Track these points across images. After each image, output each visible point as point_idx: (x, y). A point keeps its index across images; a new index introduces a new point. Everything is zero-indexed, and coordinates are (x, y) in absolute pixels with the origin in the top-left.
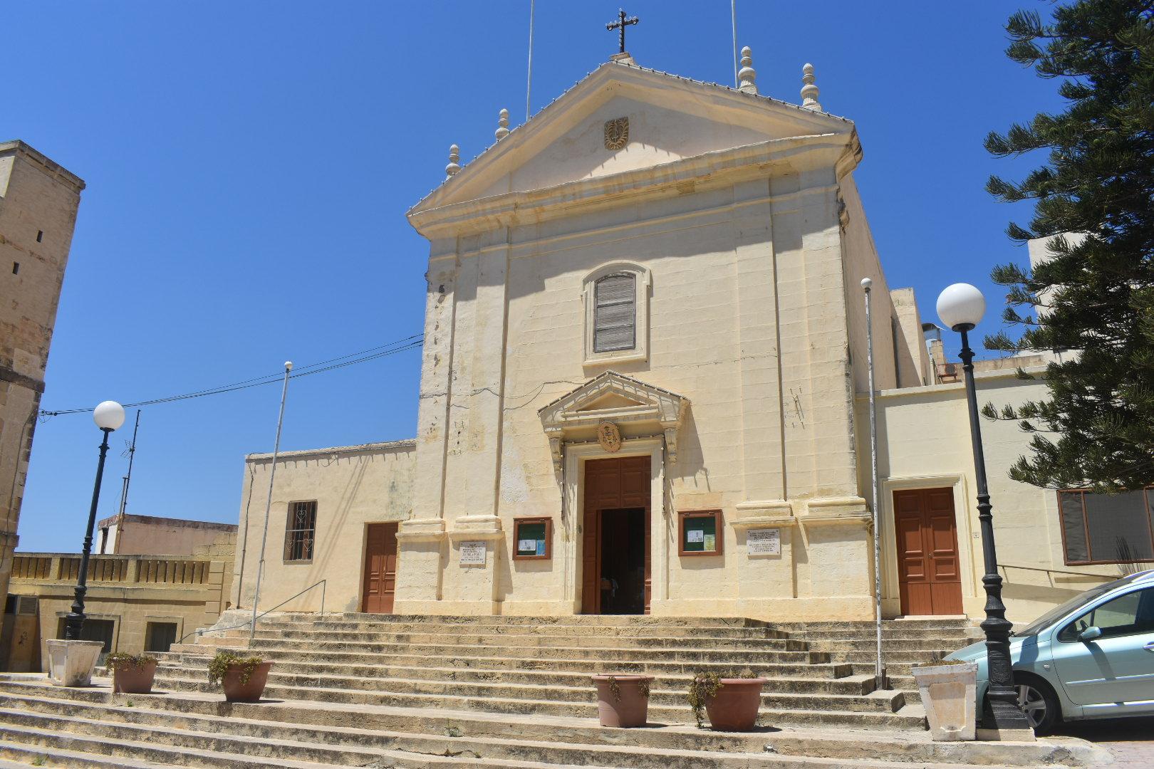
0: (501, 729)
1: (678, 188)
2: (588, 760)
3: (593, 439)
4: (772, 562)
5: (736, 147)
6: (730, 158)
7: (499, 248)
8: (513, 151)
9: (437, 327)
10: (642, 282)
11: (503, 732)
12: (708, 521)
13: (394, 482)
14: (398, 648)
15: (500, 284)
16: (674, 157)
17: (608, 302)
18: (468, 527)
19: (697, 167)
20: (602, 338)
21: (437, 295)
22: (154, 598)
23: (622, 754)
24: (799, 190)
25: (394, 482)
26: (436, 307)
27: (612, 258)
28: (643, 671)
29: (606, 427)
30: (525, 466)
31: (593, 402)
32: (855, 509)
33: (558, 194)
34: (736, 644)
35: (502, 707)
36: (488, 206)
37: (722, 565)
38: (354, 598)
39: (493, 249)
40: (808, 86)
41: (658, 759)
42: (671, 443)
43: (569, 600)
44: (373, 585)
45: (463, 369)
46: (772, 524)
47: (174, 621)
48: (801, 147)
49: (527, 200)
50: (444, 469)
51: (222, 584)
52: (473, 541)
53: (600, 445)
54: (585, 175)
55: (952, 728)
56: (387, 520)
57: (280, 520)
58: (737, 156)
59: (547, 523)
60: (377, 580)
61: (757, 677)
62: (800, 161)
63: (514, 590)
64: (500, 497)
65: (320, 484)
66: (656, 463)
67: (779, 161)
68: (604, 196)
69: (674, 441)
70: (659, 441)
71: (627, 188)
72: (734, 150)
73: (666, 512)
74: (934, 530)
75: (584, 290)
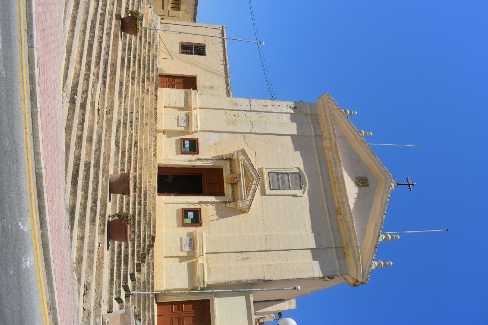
0: (109, 133)
1: (339, 208)
2: (96, 169)
3: (232, 172)
4: (179, 247)
6: (352, 230)
8: (354, 138)
9: (279, 106)
10: (298, 192)
11: (108, 134)
12: (197, 220)
13: (213, 88)
15: (297, 133)
16: (352, 206)
17: (290, 178)
18: (194, 119)
20: (275, 176)
21: (293, 106)
24: (338, 260)
26: (288, 106)
29: (237, 177)
30: (220, 143)
31: (248, 172)
32: (202, 282)
33: (336, 157)
34: (144, 232)
35: (118, 133)
36: (331, 127)
37: (178, 226)
38: (165, 71)
39: (312, 129)
42: (230, 205)
43: (164, 162)
45: (261, 117)
46: (196, 248)
48: (356, 260)
49: (333, 144)
51: (171, 16)
52: (189, 121)
54: (345, 169)
56: (198, 85)
57: (198, 40)
59: (196, 152)
60: (172, 81)
62: (350, 260)
63: (168, 138)
64: (208, 133)
65: (213, 57)
66: (221, 199)
68: (335, 176)
69: (231, 206)
73: (201, 203)
74: (193, 316)
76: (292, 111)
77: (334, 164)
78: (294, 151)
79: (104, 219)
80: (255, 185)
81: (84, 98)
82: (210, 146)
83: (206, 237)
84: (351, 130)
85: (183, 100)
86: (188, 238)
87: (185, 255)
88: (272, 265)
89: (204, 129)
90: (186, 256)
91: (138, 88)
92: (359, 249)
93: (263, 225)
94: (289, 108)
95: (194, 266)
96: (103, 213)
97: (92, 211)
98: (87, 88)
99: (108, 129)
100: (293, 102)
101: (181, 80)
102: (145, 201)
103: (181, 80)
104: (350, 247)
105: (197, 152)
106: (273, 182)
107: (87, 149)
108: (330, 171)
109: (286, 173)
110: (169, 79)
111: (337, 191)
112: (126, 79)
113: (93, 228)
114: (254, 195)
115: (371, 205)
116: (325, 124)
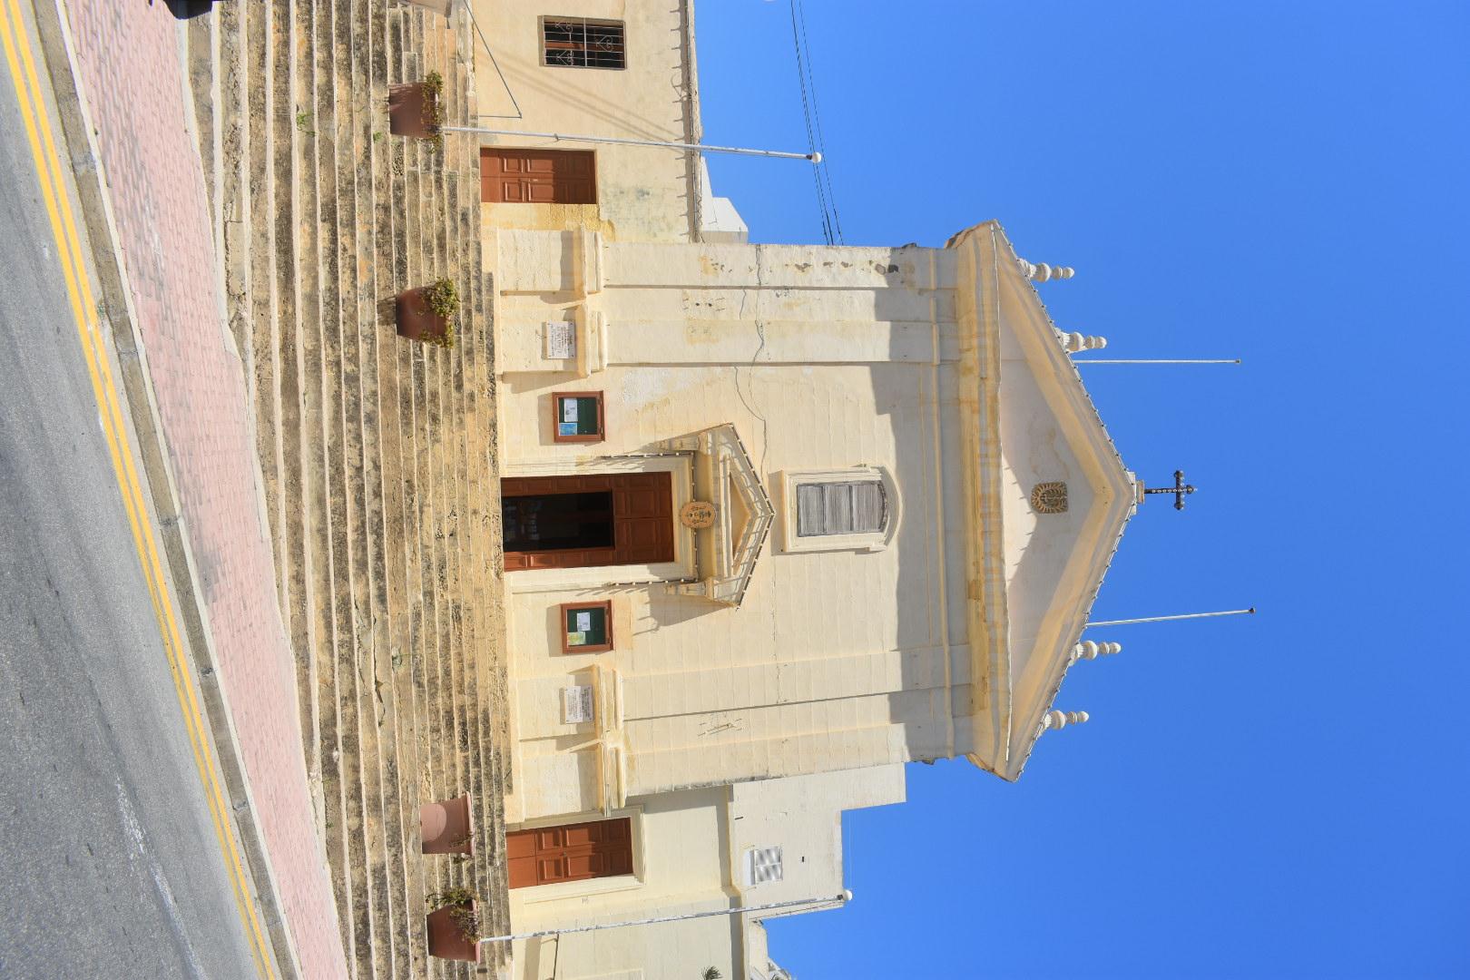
1: (976, 581)
2: (393, 850)
3: (696, 496)
6: (999, 648)
7: (935, 350)
8: (1050, 368)
9: (845, 265)
10: (873, 539)
11: (404, 722)
12: (600, 636)
13: (648, 194)
14: (461, 415)
15: (890, 356)
16: (1010, 571)
17: (854, 499)
18: (592, 332)
19: (995, 607)
20: (813, 494)
21: (886, 263)
24: (954, 717)
25: (648, 194)
26: (871, 262)
27: (906, 501)
28: (461, 751)
29: (709, 514)
30: (667, 402)
31: (740, 494)
32: (614, 798)
33: (990, 435)
35: (418, 646)
36: (989, 342)
37: (551, 654)
39: (935, 342)
40: (1063, 718)
42: (688, 590)
44: (514, 162)
45: (789, 306)
46: (598, 715)
48: (999, 725)
49: (989, 394)
50: (664, 287)
53: (689, 500)
54: (1009, 462)
58: (1000, 656)
60: (520, 169)
61: (437, 685)
62: (984, 720)
64: (630, 368)
65: (649, 73)
66: (666, 569)
67: (988, 699)
68: (979, 492)
69: (691, 593)
70: (691, 572)
71: (984, 523)
73: (610, 586)
76: (881, 282)
79: (422, 945)
81: (348, 719)
83: (624, 681)
84: (1045, 344)
86: (579, 688)
92: (1009, 699)
93: (772, 637)
94: (874, 272)
97: (398, 953)
98: (351, 687)
100: (889, 250)
104: (988, 689)
106: (807, 514)
107: (372, 830)
114: (754, 567)
115: (1062, 563)
116: (975, 329)
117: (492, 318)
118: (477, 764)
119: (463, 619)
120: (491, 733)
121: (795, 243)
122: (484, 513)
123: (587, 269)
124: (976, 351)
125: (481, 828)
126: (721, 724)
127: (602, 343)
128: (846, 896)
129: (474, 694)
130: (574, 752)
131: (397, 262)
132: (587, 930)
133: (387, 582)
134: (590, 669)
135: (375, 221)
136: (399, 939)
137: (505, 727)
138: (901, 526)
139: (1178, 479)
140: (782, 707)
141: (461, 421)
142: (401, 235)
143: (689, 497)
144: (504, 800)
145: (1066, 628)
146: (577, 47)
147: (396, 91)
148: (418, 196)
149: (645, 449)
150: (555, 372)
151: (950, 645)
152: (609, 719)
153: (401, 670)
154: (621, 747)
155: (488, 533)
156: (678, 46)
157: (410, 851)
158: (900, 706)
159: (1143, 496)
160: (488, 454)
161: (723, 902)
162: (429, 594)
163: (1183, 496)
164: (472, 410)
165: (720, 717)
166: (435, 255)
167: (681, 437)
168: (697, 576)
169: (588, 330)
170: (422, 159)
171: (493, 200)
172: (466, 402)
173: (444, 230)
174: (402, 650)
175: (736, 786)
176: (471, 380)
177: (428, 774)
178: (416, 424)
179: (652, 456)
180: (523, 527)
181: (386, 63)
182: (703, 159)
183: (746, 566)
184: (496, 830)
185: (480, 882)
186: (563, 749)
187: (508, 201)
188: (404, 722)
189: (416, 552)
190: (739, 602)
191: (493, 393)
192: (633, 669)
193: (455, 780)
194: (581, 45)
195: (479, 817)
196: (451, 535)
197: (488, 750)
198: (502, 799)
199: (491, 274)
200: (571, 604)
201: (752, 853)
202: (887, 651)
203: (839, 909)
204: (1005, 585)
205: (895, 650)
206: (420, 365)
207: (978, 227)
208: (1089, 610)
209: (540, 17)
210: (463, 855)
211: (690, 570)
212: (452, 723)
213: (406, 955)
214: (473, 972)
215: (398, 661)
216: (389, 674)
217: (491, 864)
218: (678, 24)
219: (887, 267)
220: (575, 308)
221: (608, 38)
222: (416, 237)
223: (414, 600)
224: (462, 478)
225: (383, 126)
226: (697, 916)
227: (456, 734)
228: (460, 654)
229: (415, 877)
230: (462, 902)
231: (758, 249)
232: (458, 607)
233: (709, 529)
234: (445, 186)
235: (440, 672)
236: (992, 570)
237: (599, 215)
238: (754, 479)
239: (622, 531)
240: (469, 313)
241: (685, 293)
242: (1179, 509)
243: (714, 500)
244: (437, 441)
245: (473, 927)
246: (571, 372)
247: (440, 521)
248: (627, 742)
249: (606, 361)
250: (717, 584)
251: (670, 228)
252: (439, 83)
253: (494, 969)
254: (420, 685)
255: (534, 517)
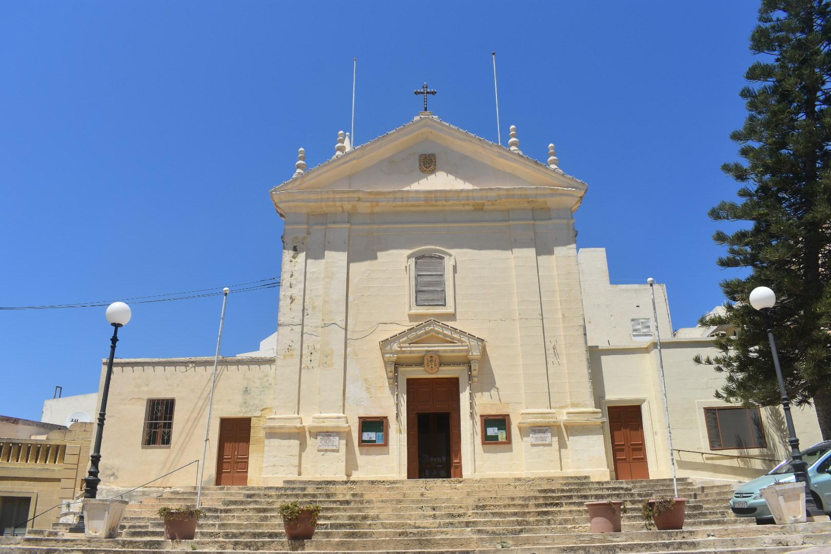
0: (539, 540)
1: (473, 205)
3: (421, 364)
4: (546, 448)
5: (517, 187)
6: (512, 193)
8: (355, 161)
9: (292, 276)
10: (448, 263)
11: (541, 541)
12: (502, 422)
13: (247, 388)
14: (364, 501)
15: (344, 251)
16: (468, 186)
17: (425, 273)
18: (324, 422)
20: (422, 296)
21: (292, 253)
22: (8, 476)
23: (639, 545)
24: (551, 219)
25: (247, 388)
26: (291, 261)
28: (562, 507)
29: (431, 357)
30: (366, 380)
33: (391, 196)
35: (498, 532)
36: (338, 196)
37: (511, 451)
38: (211, 475)
39: (337, 226)
40: (552, 158)
41: (661, 545)
42: (475, 370)
43: (403, 475)
44: (225, 465)
45: (314, 308)
46: (546, 424)
47: (27, 495)
48: (555, 194)
49: (368, 197)
51: (78, 464)
52: (328, 432)
54: (407, 186)
55: (795, 517)
56: (241, 415)
57: (139, 413)
58: (516, 192)
59: (384, 420)
60: (229, 462)
61: (522, 520)
62: (553, 202)
63: (359, 468)
64: (346, 401)
65: (178, 385)
67: (541, 200)
68: (423, 203)
69: (477, 368)
72: (515, 188)
73: (472, 415)
74: (630, 430)
75: (408, 263)
76: (302, 256)
77: (402, 201)
78: (377, 260)
79: (675, 534)
80: (444, 329)
82: (371, 397)
83: (527, 408)
85: (285, 442)
87: (557, 440)
88: (563, 315)
89: (340, 406)
90: (559, 438)
91: (372, 509)
92: (540, 188)
94: (296, 260)
95: (572, 427)
96: (667, 535)
97: (680, 548)
99: (533, 542)
100: (284, 251)
101: (227, 446)
102: (556, 491)
103: (227, 446)
104: (535, 199)
105: (506, 417)
108: (412, 209)
109: (416, 279)
110: (224, 468)
111: (448, 203)
112: (380, 528)
113: (703, 544)
116: (331, 203)
117: (310, 481)
118: (570, 497)
119: (484, 504)
120: (553, 488)
121: (278, 304)
122: (423, 490)
123: (287, 424)
124: (344, 203)
125: (609, 496)
126: (553, 352)
127: (331, 417)
128: (650, 281)
129: (529, 498)
130: (568, 438)
131: (270, 538)
132: (670, 433)
133: (456, 550)
134: (520, 428)
135: (243, 551)
136: (671, 547)
137: (550, 480)
138: (441, 247)
139: (419, 93)
140: (544, 316)
141: (368, 502)
142: (255, 535)
143: (422, 368)
144: (593, 481)
145: (501, 155)
146: (161, 426)
147: (168, 535)
148: (233, 524)
149: (393, 393)
150: (347, 445)
151: (509, 220)
152: (549, 418)
153: (510, 542)
154: (565, 411)
155: (438, 488)
156: (132, 369)
157: (618, 539)
158: (544, 249)
159: (426, 113)
160: (389, 486)
161: (655, 353)
162: (467, 524)
163: (429, 90)
164: (362, 495)
165: (549, 353)
166: (269, 515)
167: (386, 373)
168: (467, 364)
169: (323, 424)
170: (212, 520)
171: (246, 478)
172: (357, 499)
173: (255, 509)
174: (499, 542)
175: (589, 344)
176: (345, 495)
177: (574, 528)
178: (367, 529)
179: (397, 389)
180: (438, 466)
181: (151, 541)
182: (237, 355)
183: (461, 336)
184: (610, 486)
185: (641, 497)
186: (567, 445)
187: (247, 469)
188: (541, 542)
189: (441, 531)
190: (482, 340)
191: (354, 482)
192: (521, 403)
193: (579, 511)
194: (160, 424)
195: (602, 497)
196: (434, 510)
197: (563, 491)
198: (592, 482)
199: (284, 482)
200: (482, 438)
201: (634, 335)
202: (512, 256)
203: (666, 286)
204: (476, 189)
205: (512, 252)
206: (332, 525)
207: (274, 201)
208: (491, 143)
209: (143, 448)
210: (622, 507)
211: (464, 368)
212: (545, 512)
213: (681, 543)
214: (696, 502)
215: (504, 545)
216: (512, 550)
217: (630, 490)
218: (151, 368)
219: (295, 252)
220: (310, 432)
221: (157, 408)
222: (257, 526)
223: (470, 534)
224: (401, 502)
225: (188, 544)
226: (662, 367)
227: (552, 509)
228: (505, 506)
229: (634, 537)
230: (650, 508)
231: (281, 325)
232: (477, 507)
233: (440, 357)
234: (230, 507)
235: (514, 519)
236: (467, 197)
237: (257, 417)
238: (412, 331)
239: (440, 408)
240: (305, 495)
241: (304, 368)
242: (436, 93)
243: (423, 354)
244: (378, 516)
245: (665, 502)
246: (347, 435)
247: (425, 517)
248: (562, 407)
249: (341, 415)
250: (472, 353)
251: (267, 376)
252: (165, 509)
253: (695, 489)
254: (521, 531)
255: (432, 459)
